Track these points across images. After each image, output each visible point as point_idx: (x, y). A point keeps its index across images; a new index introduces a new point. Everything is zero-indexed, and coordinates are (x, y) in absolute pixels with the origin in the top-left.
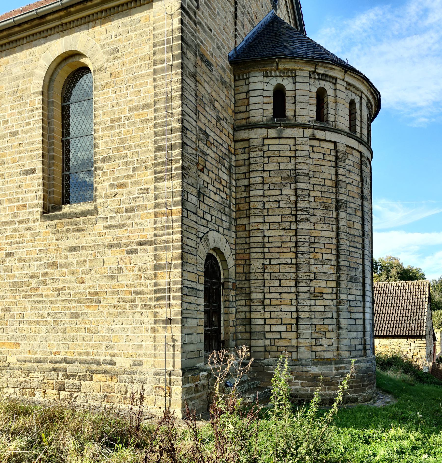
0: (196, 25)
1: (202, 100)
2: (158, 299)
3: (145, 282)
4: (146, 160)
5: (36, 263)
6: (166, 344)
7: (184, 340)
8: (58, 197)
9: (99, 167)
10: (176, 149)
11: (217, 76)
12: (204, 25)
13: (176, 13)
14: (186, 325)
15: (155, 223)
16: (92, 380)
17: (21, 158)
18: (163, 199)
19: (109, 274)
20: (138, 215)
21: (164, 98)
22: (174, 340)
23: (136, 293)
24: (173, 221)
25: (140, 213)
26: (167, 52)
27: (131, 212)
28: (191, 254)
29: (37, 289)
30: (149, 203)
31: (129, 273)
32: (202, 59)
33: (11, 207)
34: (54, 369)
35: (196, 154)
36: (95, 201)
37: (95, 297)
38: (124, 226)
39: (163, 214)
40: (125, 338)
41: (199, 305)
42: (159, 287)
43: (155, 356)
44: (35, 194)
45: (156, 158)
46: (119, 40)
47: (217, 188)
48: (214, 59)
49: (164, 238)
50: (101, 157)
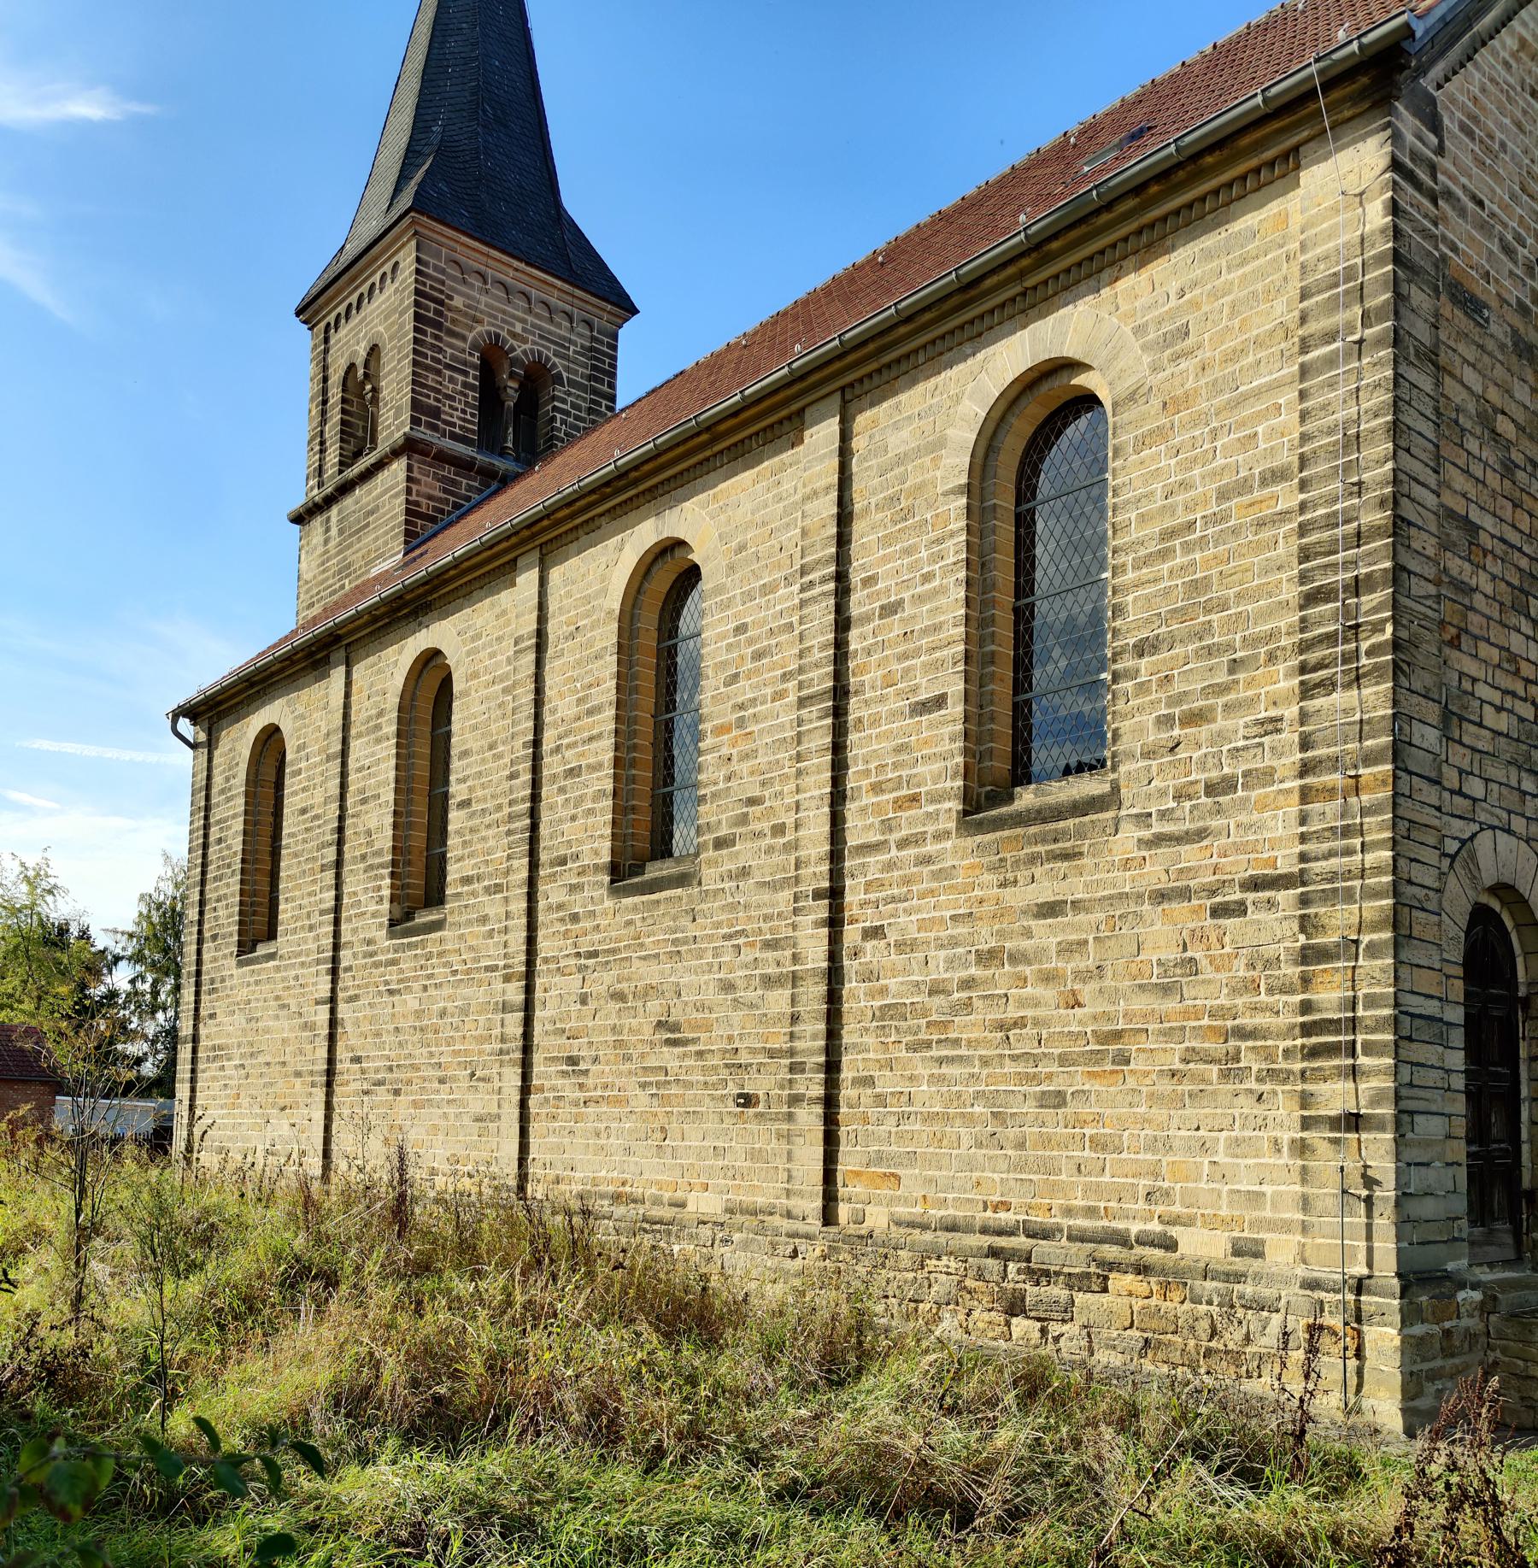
0: (1436, 204)
1: (1456, 422)
2: (1313, 1053)
3: (1271, 999)
4: (1272, 636)
5: (942, 954)
6: (1344, 1192)
7: (1403, 1182)
8: (1001, 765)
9: (1126, 670)
10: (1372, 590)
11: (1501, 336)
12: (1459, 193)
13: (1377, 186)
14: (1410, 1135)
15: (1303, 820)
16: (1105, 1290)
17: (907, 671)
18: (1329, 746)
19: (1154, 980)
20: (1248, 799)
21: (1336, 443)
22: (1369, 1182)
23: (1242, 1033)
24: (1364, 812)
25: (1254, 794)
26: (1347, 306)
27: (1225, 793)
28: (1423, 909)
29: (944, 1025)
30: (1283, 761)
31: (1219, 976)
32: (1454, 299)
33: (878, 804)
34: (994, 1253)
35: (1439, 596)
36: (1114, 769)
37: (1112, 1048)
38: (1201, 834)
39: (1331, 792)
40: (1206, 1168)
41: (1448, 1071)
42: (1316, 1017)
43: (1305, 1228)
44: (943, 764)
45: (1304, 625)
46: (1189, 301)
47: (1506, 692)
48: (1492, 288)
49: (1335, 863)
50: (1131, 641)
